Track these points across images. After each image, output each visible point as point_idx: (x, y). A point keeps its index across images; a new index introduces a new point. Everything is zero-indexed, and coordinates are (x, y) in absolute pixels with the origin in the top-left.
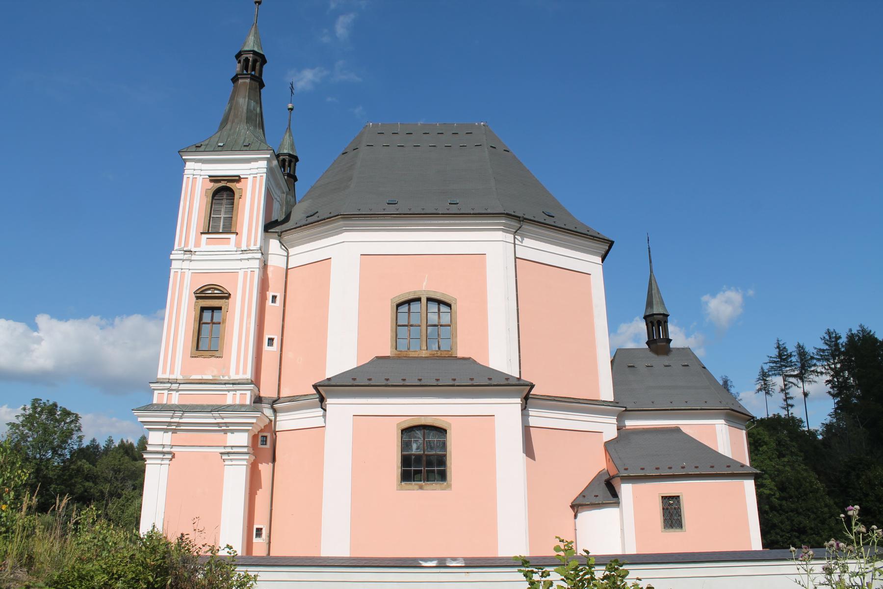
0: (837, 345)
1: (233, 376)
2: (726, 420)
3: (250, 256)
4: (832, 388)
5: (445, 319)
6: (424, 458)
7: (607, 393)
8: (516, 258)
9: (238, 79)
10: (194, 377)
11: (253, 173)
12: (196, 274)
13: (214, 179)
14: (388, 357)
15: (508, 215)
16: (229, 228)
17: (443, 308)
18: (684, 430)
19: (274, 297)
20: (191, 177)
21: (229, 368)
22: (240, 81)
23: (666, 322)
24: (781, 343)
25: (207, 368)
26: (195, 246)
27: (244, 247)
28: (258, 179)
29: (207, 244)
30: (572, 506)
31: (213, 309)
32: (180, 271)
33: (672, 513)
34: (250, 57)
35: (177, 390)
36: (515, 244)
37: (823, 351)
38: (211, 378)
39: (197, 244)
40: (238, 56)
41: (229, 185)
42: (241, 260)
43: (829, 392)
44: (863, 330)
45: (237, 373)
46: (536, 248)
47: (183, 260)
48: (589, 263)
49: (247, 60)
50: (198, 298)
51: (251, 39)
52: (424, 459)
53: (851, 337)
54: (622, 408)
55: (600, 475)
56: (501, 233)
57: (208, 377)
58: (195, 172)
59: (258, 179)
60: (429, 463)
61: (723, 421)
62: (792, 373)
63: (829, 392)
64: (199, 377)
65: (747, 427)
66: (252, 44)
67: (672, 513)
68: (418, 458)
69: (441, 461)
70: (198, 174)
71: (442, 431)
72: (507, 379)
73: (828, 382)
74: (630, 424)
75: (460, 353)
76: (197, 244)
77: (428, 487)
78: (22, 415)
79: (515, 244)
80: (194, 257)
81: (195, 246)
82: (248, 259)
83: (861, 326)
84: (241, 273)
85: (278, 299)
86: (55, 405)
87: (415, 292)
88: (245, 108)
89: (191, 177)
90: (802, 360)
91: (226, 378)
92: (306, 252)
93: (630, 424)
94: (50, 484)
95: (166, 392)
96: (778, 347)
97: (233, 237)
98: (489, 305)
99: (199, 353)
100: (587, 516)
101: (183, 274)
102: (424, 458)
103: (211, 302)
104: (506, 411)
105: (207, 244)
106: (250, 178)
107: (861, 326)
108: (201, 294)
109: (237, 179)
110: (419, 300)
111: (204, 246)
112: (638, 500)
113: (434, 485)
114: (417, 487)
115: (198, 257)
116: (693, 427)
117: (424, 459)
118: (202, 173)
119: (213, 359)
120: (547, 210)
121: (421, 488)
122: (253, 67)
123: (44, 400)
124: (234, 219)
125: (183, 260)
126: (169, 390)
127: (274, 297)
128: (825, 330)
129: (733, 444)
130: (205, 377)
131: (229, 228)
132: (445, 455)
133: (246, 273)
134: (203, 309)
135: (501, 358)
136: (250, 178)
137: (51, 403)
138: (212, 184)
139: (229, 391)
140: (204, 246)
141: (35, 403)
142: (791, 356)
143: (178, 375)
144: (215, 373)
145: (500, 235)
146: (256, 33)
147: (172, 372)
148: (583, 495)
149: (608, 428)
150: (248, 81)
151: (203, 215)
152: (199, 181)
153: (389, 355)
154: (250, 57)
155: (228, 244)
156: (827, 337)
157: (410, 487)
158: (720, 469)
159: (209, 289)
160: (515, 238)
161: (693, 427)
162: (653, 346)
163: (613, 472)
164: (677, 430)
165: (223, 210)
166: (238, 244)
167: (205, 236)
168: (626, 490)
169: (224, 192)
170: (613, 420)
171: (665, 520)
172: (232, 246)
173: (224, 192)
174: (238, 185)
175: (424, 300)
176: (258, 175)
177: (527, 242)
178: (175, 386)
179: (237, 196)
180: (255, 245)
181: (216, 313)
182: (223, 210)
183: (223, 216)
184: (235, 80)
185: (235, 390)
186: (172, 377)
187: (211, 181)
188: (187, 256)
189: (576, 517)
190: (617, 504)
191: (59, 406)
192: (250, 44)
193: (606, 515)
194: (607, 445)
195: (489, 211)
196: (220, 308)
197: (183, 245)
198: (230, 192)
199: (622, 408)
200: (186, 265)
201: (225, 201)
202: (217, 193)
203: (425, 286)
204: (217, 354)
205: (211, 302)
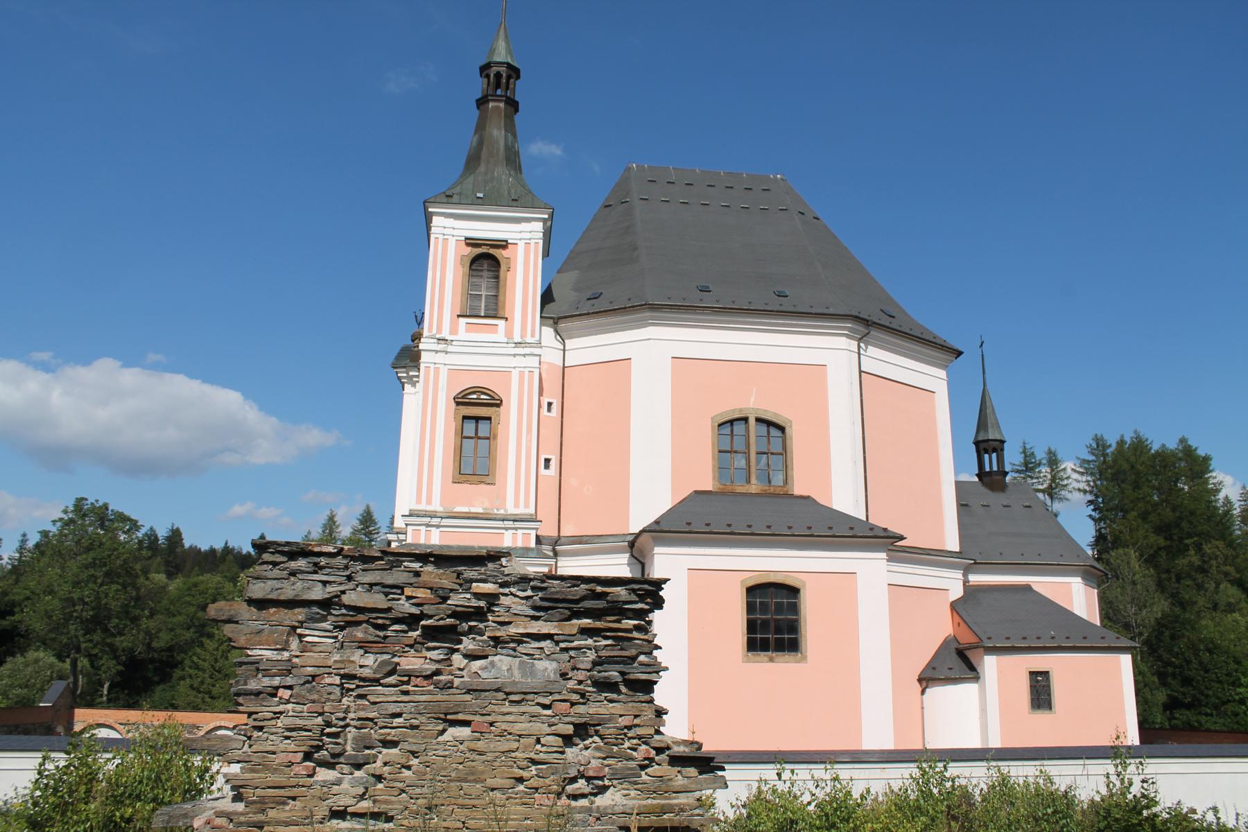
0: (1105, 455)
1: (511, 510)
2: (1083, 579)
3: (527, 351)
4: (1094, 510)
5: (776, 446)
6: (772, 624)
7: (953, 544)
8: (861, 372)
9: (488, 101)
10: (458, 509)
11: (523, 236)
12: (454, 372)
13: (471, 242)
14: (710, 492)
15: (857, 319)
16: (495, 310)
17: (774, 432)
18: (1035, 587)
19: (550, 404)
20: (441, 237)
21: (504, 499)
22: (491, 104)
23: (1002, 450)
24: (1028, 447)
25: (475, 499)
26: (451, 333)
27: (517, 339)
28: (532, 246)
29: (467, 331)
30: (920, 680)
31: (477, 419)
32: (432, 366)
33: (1040, 693)
34: (503, 70)
35: (438, 526)
36: (859, 354)
37: (1088, 462)
38: (481, 511)
39: (454, 330)
40: (485, 69)
41: (492, 251)
42: (514, 355)
43: (1090, 516)
44: (1138, 437)
45: (516, 505)
46: (884, 361)
47: (437, 352)
48: (932, 378)
49: (498, 75)
50: (458, 404)
51: (501, 45)
52: (773, 622)
53: (1121, 443)
54: (970, 557)
55: (946, 644)
56: (844, 339)
57: (479, 510)
58: (446, 231)
59: (532, 246)
60: (778, 630)
61: (1079, 579)
62: (1040, 487)
63: (1090, 516)
64: (465, 509)
65: (1099, 586)
66: (503, 52)
67: (1040, 693)
68: (765, 623)
69: (793, 627)
70: (451, 233)
71: (794, 591)
72: (871, 529)
73: (1090, 502)
74: (975, 579)
75: (798, 491)
76: (454, 330)
77: (781, 659)
78: (61, 519)
79: (859, 354)
80: (450, 348)
81: (451, 333)
82: (524, 355)
83: (1135, 432)
84: (515, 375)
85: (554, 407)
86: (106, 507)
87: (741, 410)
88: (502, 143)
89: (441, 237)
90: (1052, 470)
91: (502, 512)
92: (593, 347)
93: (975, 579)
94: (109, 618)
95: (423, 528)
96: (1024, 452)
97: (501, 323)
98: (832, 432)
99: (463, 478)
100: (940, 694)
101: (437, 370)
102: (772, 624)
103: (477, 410)
104: (871, 568)
105: (467, 331)
106: (521, 245)
107: (1135, 432)
108: (461, 400)
109: (503, 245)
110: (746, 419)
111: (462, 334)
112: (1002, 674)
113: (787, 656)
114: (766, 659)
115: (459, 348)
116: (1045, 584)
117: (773, 622)
118: (455, 232)
119: (483, 486)
120: (884, 308)
121: (771, 660)
122: (500, 83)
123: (91, 500)
124: (501, 298)
125: (437, 352)
126: (428, 525)
127: (550, 404)
128: (1092, 436)
129: (1089, 606)
130: (473, 510)
131: (495, 310)
132: (797, 621)
133: (521, 374)
134: (465, 418)
135: (845, 498)
136: (521, 245)
137: (101, 503)
138: (469, 249)
139: (506, 529)
140: (462, 334)
141: (80, 502)
142: (1039, 465)
143: (436, 506)
144: (487, 504)
145: (843, 342)
146: (506, 37)
147: (429, 502)
148: (931, 666)
149: (952, 584)
150: (502, 105)
151: (459, 290)
152: (452, 243)
153: (710, 488)
154: (503, 70)
155: (496, 332)
156: (1094, 445)
157: (758, 658)
158: (1070, 637)
159: (474, 393)
160: (859, 347)
161: (1045, 584)
162: (986, 479)
163: (967, 638)
164: (1027, 588)
165: (484, 286)
166: (509, 333)
167: (463, 321)
168: (990, 664)
169: (486, 261)
170: (959, 575)
171: (1032, 700)
172: (500, 336)
173: (486, 261)
174: (505, 253)
175: (752, 421)
176: (532, 242)
177: (872, 351)
178: (435, 521)
179: (503, 268)
180: (533, 336)
181: (483, 426)
182: (484, 286)
183: (484, 293)
184: (482, 102)
185: (516, 529)
186: (429, 508)
187: (468, 245)
188: (441, 347)
189: (923, 692)
190: (976, 678)
191: (110, 508)
192: (501, 55)
193: (966, 692)
194: (954, 606)
195: (831, 311)
196: (489, 419)
197: (434, 331)
198: (495, 263)
199: (970, 557)
200: (440, 358)
201: (485, 274)
202: (476, 260)
203: (754, 402)
204: (488, 479)
205: (477, 410)
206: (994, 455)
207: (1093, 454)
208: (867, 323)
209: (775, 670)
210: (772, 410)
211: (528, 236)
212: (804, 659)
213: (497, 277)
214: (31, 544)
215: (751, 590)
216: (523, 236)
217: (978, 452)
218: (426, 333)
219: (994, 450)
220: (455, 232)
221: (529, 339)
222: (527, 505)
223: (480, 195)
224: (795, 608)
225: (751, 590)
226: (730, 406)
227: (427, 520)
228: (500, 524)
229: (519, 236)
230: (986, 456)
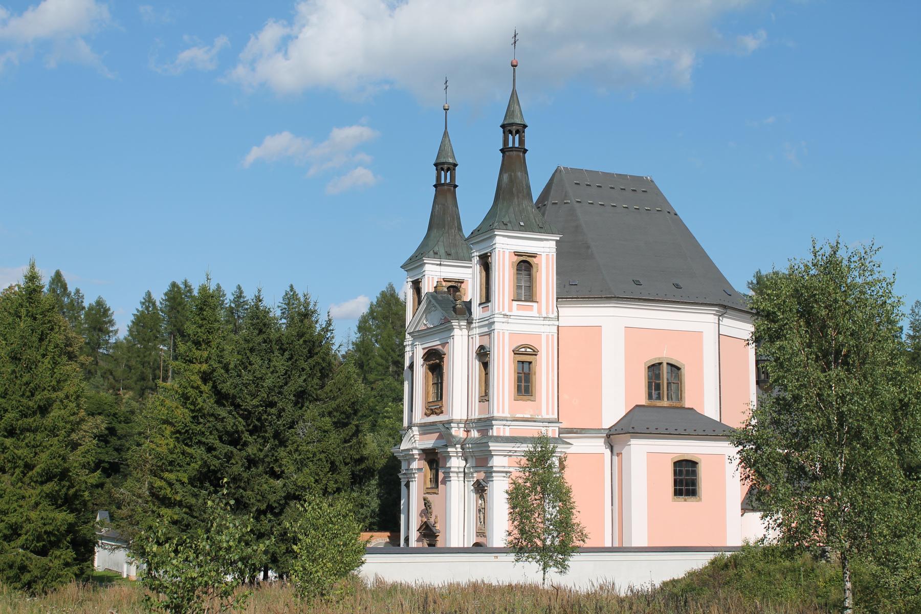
1: (545, 415)
10: (518, 416)
11: (544, 249)
13: (517, 254)
27: (544, 315)
39: (510, 309)
41: (528, 259)
45: (548, 413)
64: (521, 416)
68: (681, 481)
75: (687, 406)
76: (510, 309)
80: (510, 321)
92: (579, 315)
106: (544, 255)
109: (534, 256)
113: (693, 498)
133: (547, 336)
135: (710, 411)
147: (503, 412)
155: (532, 310)
156: (755, 282)
166: (539, 311)
167: (515, 303)
169: (525, 266)
172: (534, 313)
173: (525, 266)
177: (726, 321)
178: (509, 423)
179: (534, 270)
200: (505, 326)
206: (517, 137)
207: (753, 289)
208: (725, 307)
209: (686, 505)
210: (676, 359)
211: (548, 250)
212: (700, 500)
213: (530, 275)
214: (766, 543)
215: (675, 464)
216: (544, 249)
217: (504, 132)
218: (497, 311)
219: (517, 132)
220: (508, 247)
221: (551, 315)
222: (553, 414)
223: (522, 224)
224: (694, 473)
225: (675, 464)
226: (653, 356)
227: (504, 422)
228: (541, 424)
229: (543, 250)
230: (510, 137)
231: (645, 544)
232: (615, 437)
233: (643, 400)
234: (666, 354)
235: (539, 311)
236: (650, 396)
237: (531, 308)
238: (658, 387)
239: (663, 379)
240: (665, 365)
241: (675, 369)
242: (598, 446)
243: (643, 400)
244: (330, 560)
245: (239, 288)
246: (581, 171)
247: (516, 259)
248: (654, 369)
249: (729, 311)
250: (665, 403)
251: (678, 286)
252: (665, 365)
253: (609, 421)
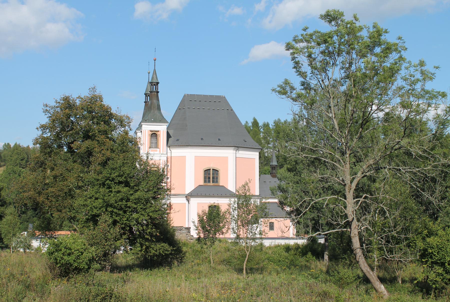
13: (151, 131)
92: (177, 152)
109: (158, 131)
166: (160, 151)
169: (154, 135)
172: (158, 152)
173: (154, 135)
179: (158, 136)
221: (164, 153)
226: (207, 167)
231: (276, 237)
232: (188, 197)
233: (202, 183)
234: (212, 166)
235: (160, 151)
236: (205, 181)
237: (157, 151)
238: (209, 178)
239: (211, 175)
240: (211, 170)
241: (216, 171)
242: (184, 200)
243: (202, 183)
244: (385, 232)
245: (254, 118)
246: (191, 95)
247: (151, 133)
248: (207, 171)
249: (239, 148)
250: (211, 184)
251: (219, 140)
252: (211, 170)
253: (188, 191)
